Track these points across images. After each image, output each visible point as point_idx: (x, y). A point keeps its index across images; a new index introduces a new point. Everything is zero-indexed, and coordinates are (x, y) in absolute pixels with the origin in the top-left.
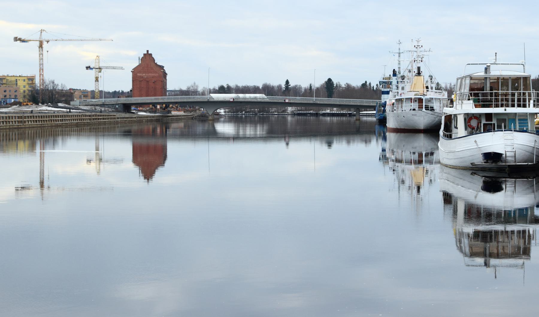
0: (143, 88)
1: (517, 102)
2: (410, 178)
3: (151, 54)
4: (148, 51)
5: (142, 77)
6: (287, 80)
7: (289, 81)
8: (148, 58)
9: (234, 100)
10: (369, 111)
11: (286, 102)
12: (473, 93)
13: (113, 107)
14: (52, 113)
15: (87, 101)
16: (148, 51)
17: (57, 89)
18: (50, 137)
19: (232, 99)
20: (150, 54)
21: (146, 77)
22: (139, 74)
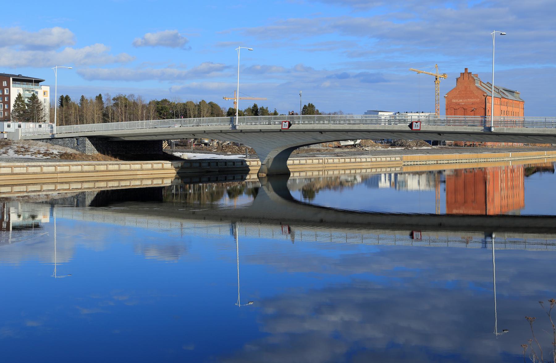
2: (442, 151)
4: (466, 69)
5: (458, 104)
15: (57, 152)
16: (466, 69)
17: (175, 172)
19: (287, 123)
21: (463, 104)
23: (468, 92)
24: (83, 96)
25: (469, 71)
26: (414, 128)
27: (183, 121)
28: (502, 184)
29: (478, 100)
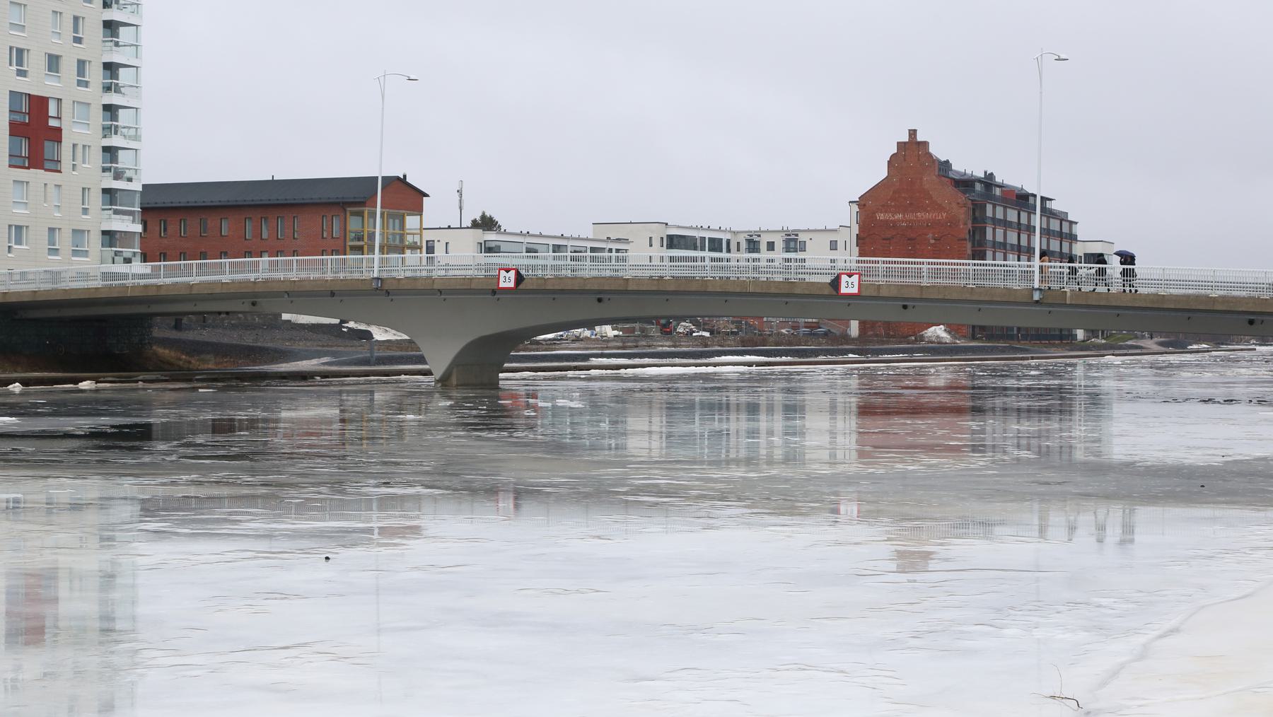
3: (925, 144)
4: (913, 133)
9: (519, 278)
11: (844, 290)
12: (194, 266)
16: (913, 133)
19: (512, 273)
21: (904, 224)
23: (918, 194)
24: (427, 196)
25: (920, 138)
26: (844, 290)
27: (295, 262)
28: (110, 392)
29: (942, 216)
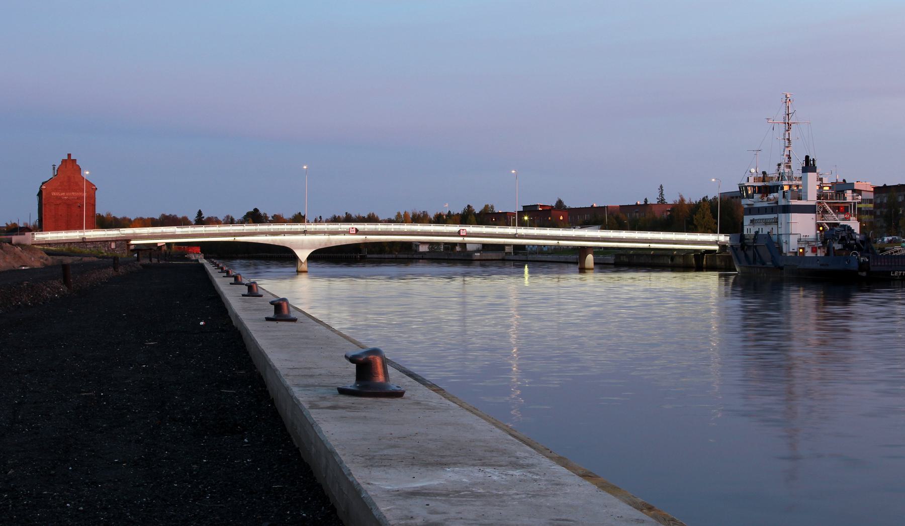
0: (61, 215)
1: (82, 229)
4: (69, 155)
5: (60, 198)
6: (200, 210)
7: (202, 212)
8: (69, 165)
10: (105, 242)
13: (104, 247)
14: (626, 285)
16: (69, 155)
18: (791, 326)
20: (73, 160)
22: (54, 194)
